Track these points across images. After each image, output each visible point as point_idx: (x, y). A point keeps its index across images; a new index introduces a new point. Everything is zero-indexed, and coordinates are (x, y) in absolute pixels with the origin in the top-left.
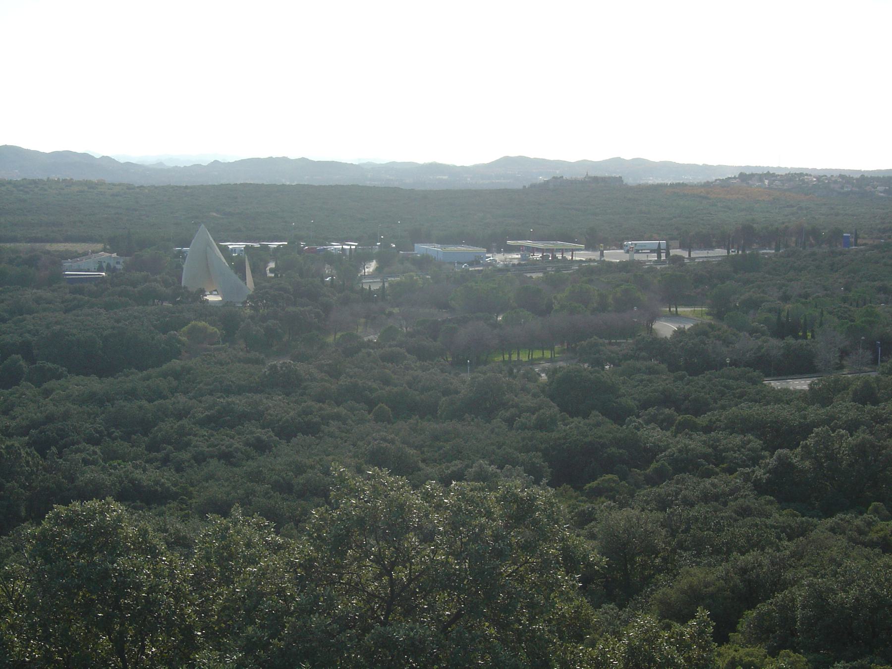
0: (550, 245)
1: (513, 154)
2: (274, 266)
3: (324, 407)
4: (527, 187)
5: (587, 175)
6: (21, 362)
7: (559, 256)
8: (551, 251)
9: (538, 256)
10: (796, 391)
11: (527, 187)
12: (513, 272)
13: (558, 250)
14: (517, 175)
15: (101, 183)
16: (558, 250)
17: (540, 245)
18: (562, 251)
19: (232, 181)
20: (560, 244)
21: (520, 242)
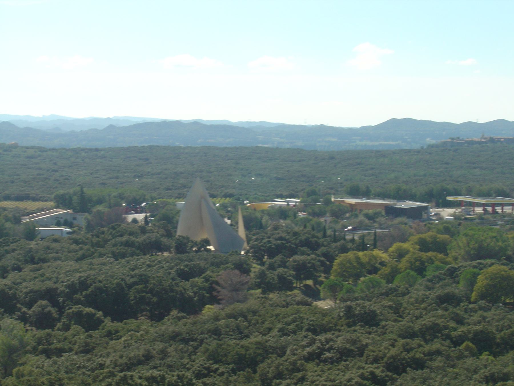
0: (491, 200)
1: (400, 116)
2: (490, 208)
3: (126, 329)
4: (425, 148)
5: (483, 136)
6: (49, 308)
7: (499, 209)
8: (493, 206)
9: (479, 210)
10: (321, 308)
11: (425, 148)
12: (12, 246)
13: (498, 205)
14: (405, 137)
15: (15, 146)
16: (498, 205)
17: (481, 200)
18: (502, 205)
19: (286, 124)
20: (500, 199)
21: (460, 198)
